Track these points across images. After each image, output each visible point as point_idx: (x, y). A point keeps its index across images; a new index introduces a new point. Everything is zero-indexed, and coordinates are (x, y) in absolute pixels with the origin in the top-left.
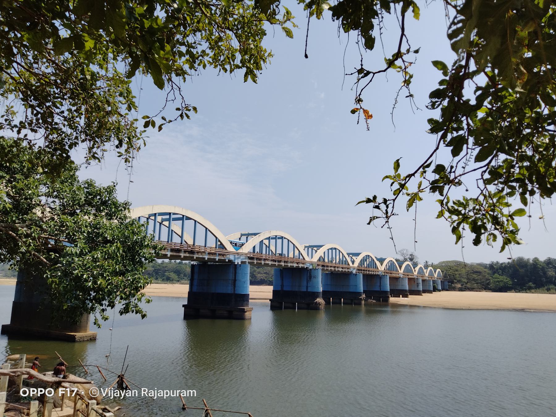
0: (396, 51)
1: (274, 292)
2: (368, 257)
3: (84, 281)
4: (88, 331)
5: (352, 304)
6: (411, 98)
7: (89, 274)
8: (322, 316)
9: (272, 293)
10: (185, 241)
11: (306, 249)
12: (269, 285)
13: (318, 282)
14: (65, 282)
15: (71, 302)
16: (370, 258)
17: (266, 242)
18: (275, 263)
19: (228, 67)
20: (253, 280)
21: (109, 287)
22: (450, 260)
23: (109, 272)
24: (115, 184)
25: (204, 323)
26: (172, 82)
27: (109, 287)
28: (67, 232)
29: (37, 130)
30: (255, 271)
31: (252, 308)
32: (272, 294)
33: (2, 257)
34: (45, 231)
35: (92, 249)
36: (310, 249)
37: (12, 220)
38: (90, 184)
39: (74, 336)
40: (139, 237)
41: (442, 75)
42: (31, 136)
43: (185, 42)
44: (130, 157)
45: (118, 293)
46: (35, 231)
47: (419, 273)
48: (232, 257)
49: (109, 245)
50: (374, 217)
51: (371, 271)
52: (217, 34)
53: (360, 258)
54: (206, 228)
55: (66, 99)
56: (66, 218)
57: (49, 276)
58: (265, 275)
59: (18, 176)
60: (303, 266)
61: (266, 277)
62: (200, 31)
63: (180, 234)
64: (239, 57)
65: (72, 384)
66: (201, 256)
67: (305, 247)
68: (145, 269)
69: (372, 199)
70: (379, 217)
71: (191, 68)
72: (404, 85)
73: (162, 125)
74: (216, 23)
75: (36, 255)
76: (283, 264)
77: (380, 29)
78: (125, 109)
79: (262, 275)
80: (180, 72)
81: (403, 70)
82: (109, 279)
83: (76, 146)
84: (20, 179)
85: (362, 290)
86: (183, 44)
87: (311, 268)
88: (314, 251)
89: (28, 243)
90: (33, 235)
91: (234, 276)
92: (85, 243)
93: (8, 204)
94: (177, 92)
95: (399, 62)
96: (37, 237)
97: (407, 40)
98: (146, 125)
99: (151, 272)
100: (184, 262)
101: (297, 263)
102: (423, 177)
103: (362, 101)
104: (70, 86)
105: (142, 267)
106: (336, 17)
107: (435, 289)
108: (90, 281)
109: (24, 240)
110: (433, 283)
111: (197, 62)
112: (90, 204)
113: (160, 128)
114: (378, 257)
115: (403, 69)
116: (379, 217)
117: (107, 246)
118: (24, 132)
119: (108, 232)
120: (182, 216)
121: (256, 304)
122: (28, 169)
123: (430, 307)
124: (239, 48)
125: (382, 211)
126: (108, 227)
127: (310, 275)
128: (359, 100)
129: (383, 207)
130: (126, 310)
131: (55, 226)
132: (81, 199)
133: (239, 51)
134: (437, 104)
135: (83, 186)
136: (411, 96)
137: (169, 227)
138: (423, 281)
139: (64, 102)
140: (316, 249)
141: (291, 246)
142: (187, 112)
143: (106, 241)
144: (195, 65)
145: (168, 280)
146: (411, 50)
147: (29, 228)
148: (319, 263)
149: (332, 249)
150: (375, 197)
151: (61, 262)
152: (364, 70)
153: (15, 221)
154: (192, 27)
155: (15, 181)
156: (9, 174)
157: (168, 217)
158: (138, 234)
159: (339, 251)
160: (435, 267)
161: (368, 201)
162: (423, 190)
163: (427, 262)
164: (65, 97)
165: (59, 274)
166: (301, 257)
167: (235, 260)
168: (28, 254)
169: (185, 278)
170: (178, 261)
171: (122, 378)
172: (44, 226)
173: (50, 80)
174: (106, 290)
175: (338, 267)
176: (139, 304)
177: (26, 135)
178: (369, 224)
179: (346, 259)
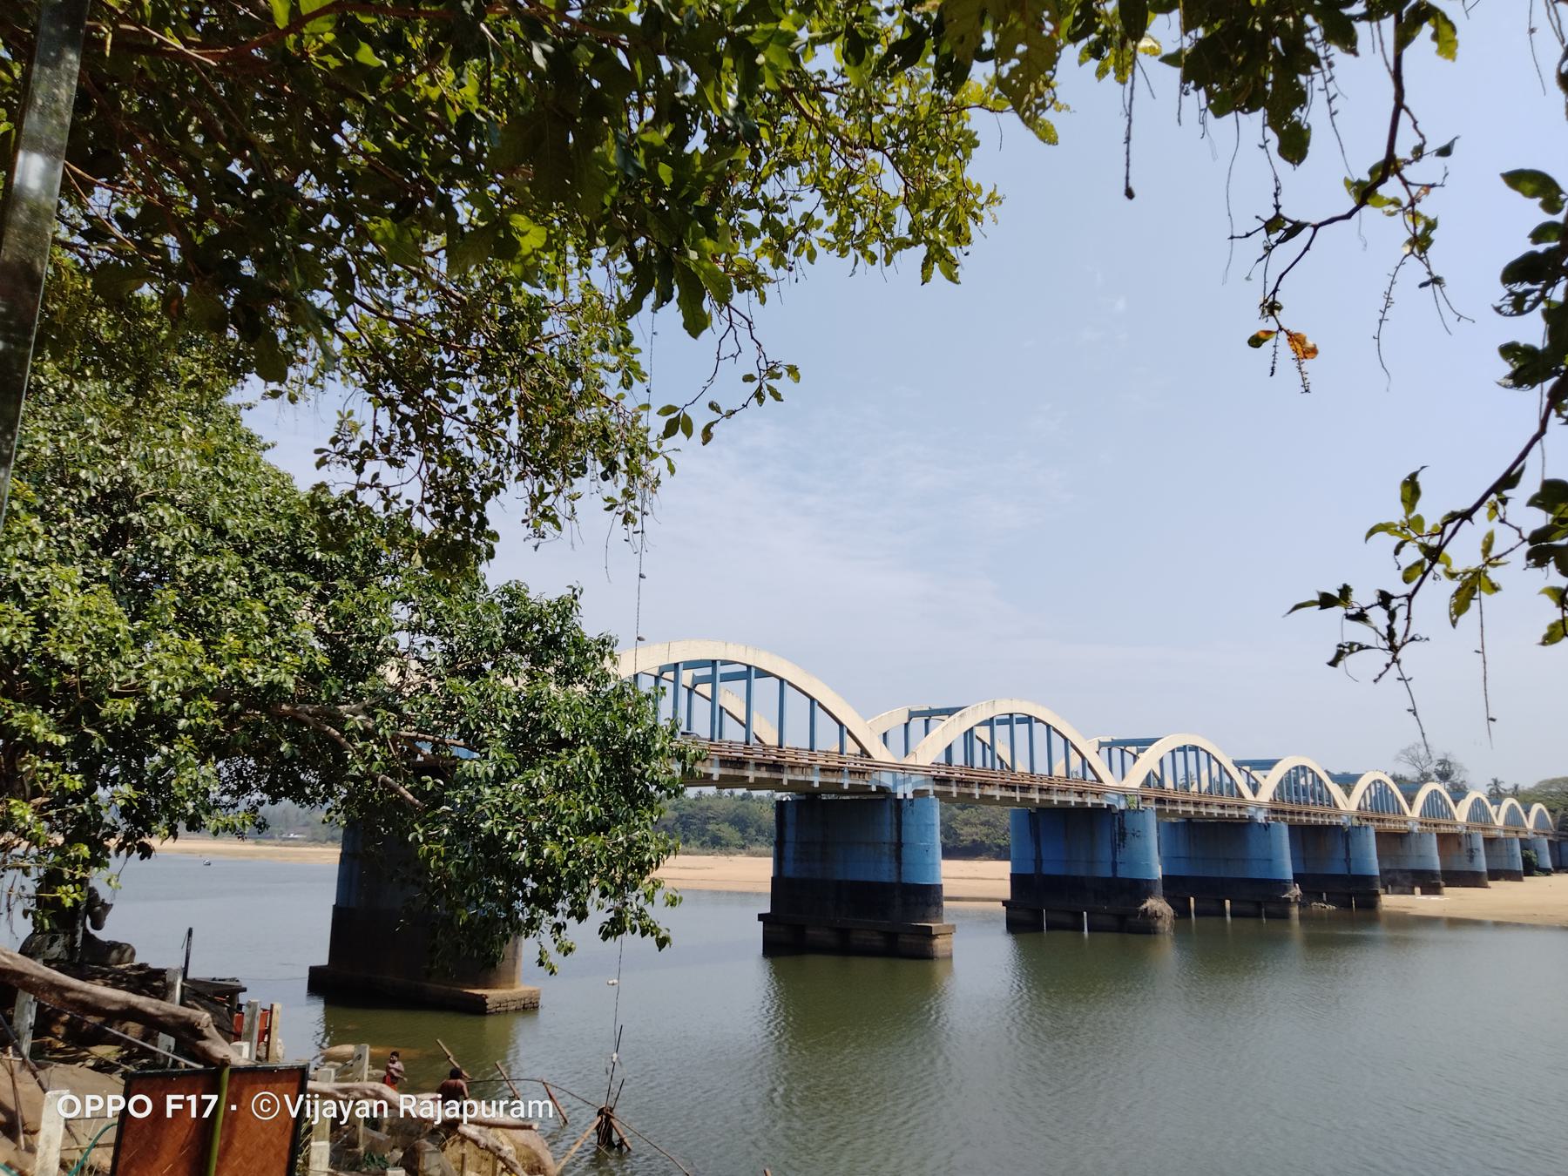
0: (1380, 155)
1: (1015, 878)
2: (1301, 772)
3: (508, 850)
4: (517, 983)
5: (1258, 916)
6: (1436, 286)
7: (518, 830)
8: (1168, 954)
9: (1009, 883)
10: (757, 737)
11: (1105, 750)
12: (998, 857)
13: (1147, 848)
14: (460, 852)
15: (478, 906)
16: (1309, 775)
17: (984, 733)
18: (1013, 794)
19: (875, 247)
20: (951, 844)
21: (570, 864)
22: (1558, 777)
23: (568, 824)
24: (577, 593)
25: (820, 966)
26: (729, 307)
27: (570, 864)
28: (462, 721)
29: (403, 461)
30: (953, 818)
31: (954, 926)
32: (1008, 884)
33: (308, 791)
34: (408, 720)
35: (527, 762)
36: (1116, 752)
37: (329, 695)
38: (514, 594)
39: (483, 999)
40: (639, 731)
41: (1541, 211)
42: (389, 476)
43: (756, 200)
44: (636, 509)
45: (594, 881)
46: (386, 724)
47: (1473, 815)
48: (886, 780)
49: (564, 751)
50: (1352, 644)
51: (1315, 815)
52: (843, 165)
53: (1276, 775)
54: (812, 700)
55: (470, 376)
56: (458, 685)
57: (421, 839)
58: (985, 830)
59: (341, 584)
60: (1097, 801)
61: (987, 836)
62: (795, 163)
63: (743, 718)
64: (903, 220)
65: (484, 1129)
66: (801, 778)
67: (1101, 745)
68: (660, 813)
69: (1337, 594)
70: (1368, 647)
71: (775, 266)
72: (1412, 252)
73: (711, 425)
74: (838, 136)
75: (389, 784)
76: (1036, 796)
77: (1329, 101)
78: (618, 383)
79: (974, 829)
80: (748, 279)
81: (1404, 209)
82: (570, 843)
83: (498, 493)
84: (346, 591)
85: (1288, 872)
86: (751, 204)
87: (1123, 807)
88: (1128, 758)
89: (368, 752)
90: (381, 731)
91: (895, 833)
92: (508, 749)
93: (319, 656)
94: (743, 334)
95: (1391, 188)
96: (389, 737)
97: (1415, 123)
98: (670, 431)
99: (670, 824)
100: (755, 793)
101: (1080, 794)
102: (1497, 518)
103: (1280, 308)
104: (478, 340)
105: (651, 808)
106: (1193, 83)
107: (1531, 868)
108: (522, 850)
109: (359, 745)
110: (1523, 848)
111: (792, 246)
112: (516, 646)
113: (707, 435)
114: (1336, 772)
115: (1405, 205)
116: (1368, 647)
117: (560, 754)
118: (371, 467)
119: (562, 716)
120: (745, 669)
121: (962, 915)
122: (364, 565)
123: (1519, 925)
124: (902, 194)
125: (1376, 629)
126: (562, 706)
127: (1122, 827)
128: (1271, 308)
129: (1378, 616)
130: (613, 928)
131: (432, 707)
132: (495, 634)
133: (904, 202)
134: (1532, 297)
135: (497, 600)
136: (1436, 281)
137: (713, 700)
138: (1490, 842)
139: (466, 384)
140: (1133, 749)
141: (1057, 742)
142: (773, 383)
143: (558, 743)
144: (786, 255)
145: (716, 844)
146: (1427, 149)
147: (369, 716)
148: (1147, 793)
149: (1183, 749)
150: (1345, 591)
151: (450, 802)
152: (1286, 219)
153: (336, 697)
154: (776, 155)
155: (333, 597)
156: (321, 579)
157: (708, 671)
158: (636, 722)
159: (1208, 754)
160: (1526, 799)
161: (1326, 601)
162: (1501, 560)
163: (1496, 782)
164: (468, 371)
165: (446, 832)
166: (1090, 776)
167: (895, 786)
168: (369, 783)
169: (760, 838)
170: (739, 792)
171: (609, 1117)
172: (406, 710)
173: (429, 332)
174: (564, 872)
175: (1207, 805)
176: (648, 908)
177: (376, 476)
178: (1333, 663)
179: (1231, 779)
